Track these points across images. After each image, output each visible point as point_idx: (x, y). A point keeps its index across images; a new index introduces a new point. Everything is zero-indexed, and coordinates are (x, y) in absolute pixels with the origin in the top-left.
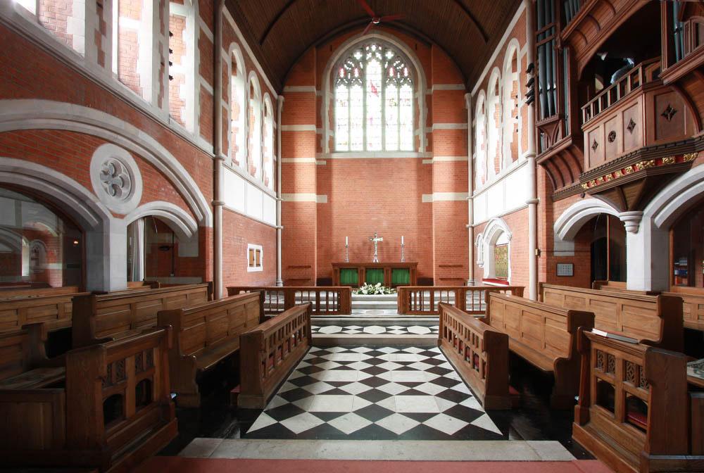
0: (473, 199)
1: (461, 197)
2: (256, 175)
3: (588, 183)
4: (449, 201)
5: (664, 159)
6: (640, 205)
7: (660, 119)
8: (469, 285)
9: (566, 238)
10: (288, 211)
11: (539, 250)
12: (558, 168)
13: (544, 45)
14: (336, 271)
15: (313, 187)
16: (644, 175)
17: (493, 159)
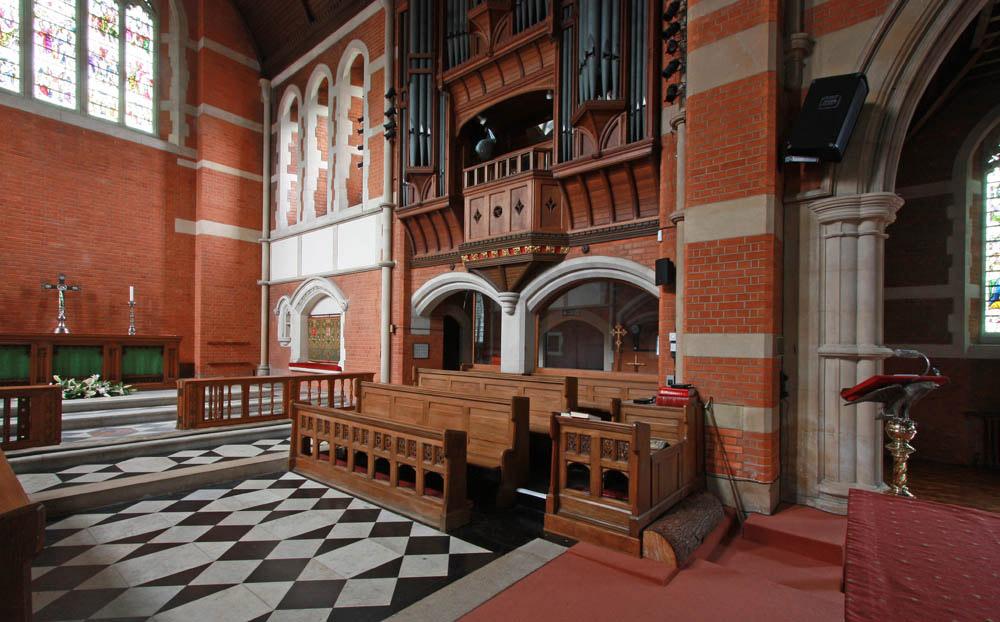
0: (269, 243)
1: (249, 236)
3: (469, 256)
4: (229, 239)
5: (548, 248)
8: (261, 374)
9: (423, 314)
11: (394, 326)
12: (420, 234)
13: (418, 75)
16: (530, 258)
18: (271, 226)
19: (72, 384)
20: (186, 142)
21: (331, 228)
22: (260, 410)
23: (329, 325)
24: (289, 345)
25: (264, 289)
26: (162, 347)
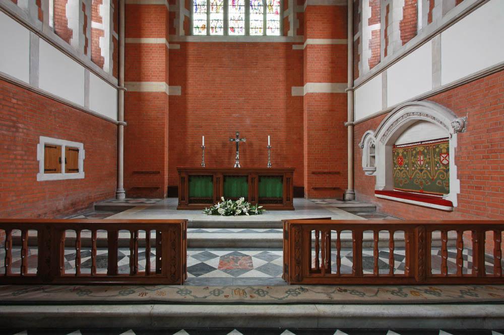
0: (353, 91)
1: (338, 88)
2: (72, 41)
10: (133, 103)
14: (183, 179)
15: (163, 74)
18: (355, 75)
19: (230, 204)
20: (297, 32)
21: (430, 43)
22: (376, 269)
23: (422, 153)
24: (375, 174)
25: (349, 128)
26: (282, 177)
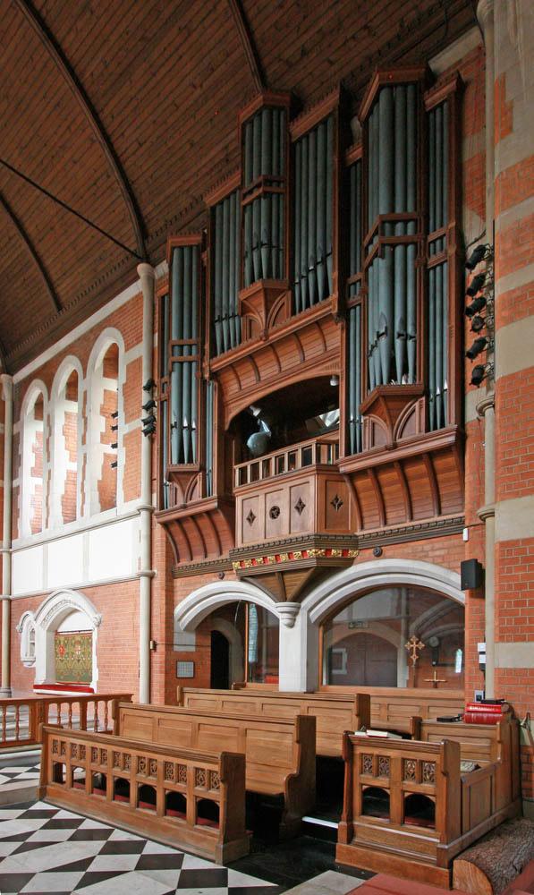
0: (10, 554)
6: (299, 597)
7: (330, 507)
9: (187, 629)
12: (184, 538)
13: (182, 363)
16: (313, 563)
17: (60, 498)
